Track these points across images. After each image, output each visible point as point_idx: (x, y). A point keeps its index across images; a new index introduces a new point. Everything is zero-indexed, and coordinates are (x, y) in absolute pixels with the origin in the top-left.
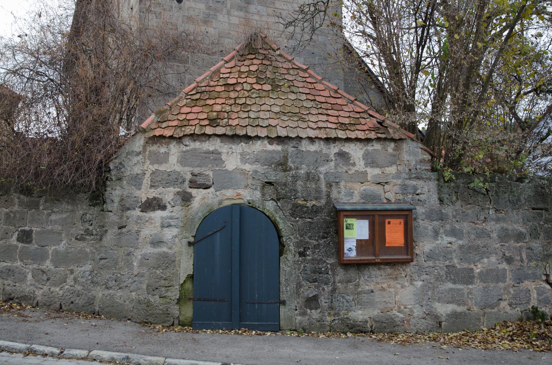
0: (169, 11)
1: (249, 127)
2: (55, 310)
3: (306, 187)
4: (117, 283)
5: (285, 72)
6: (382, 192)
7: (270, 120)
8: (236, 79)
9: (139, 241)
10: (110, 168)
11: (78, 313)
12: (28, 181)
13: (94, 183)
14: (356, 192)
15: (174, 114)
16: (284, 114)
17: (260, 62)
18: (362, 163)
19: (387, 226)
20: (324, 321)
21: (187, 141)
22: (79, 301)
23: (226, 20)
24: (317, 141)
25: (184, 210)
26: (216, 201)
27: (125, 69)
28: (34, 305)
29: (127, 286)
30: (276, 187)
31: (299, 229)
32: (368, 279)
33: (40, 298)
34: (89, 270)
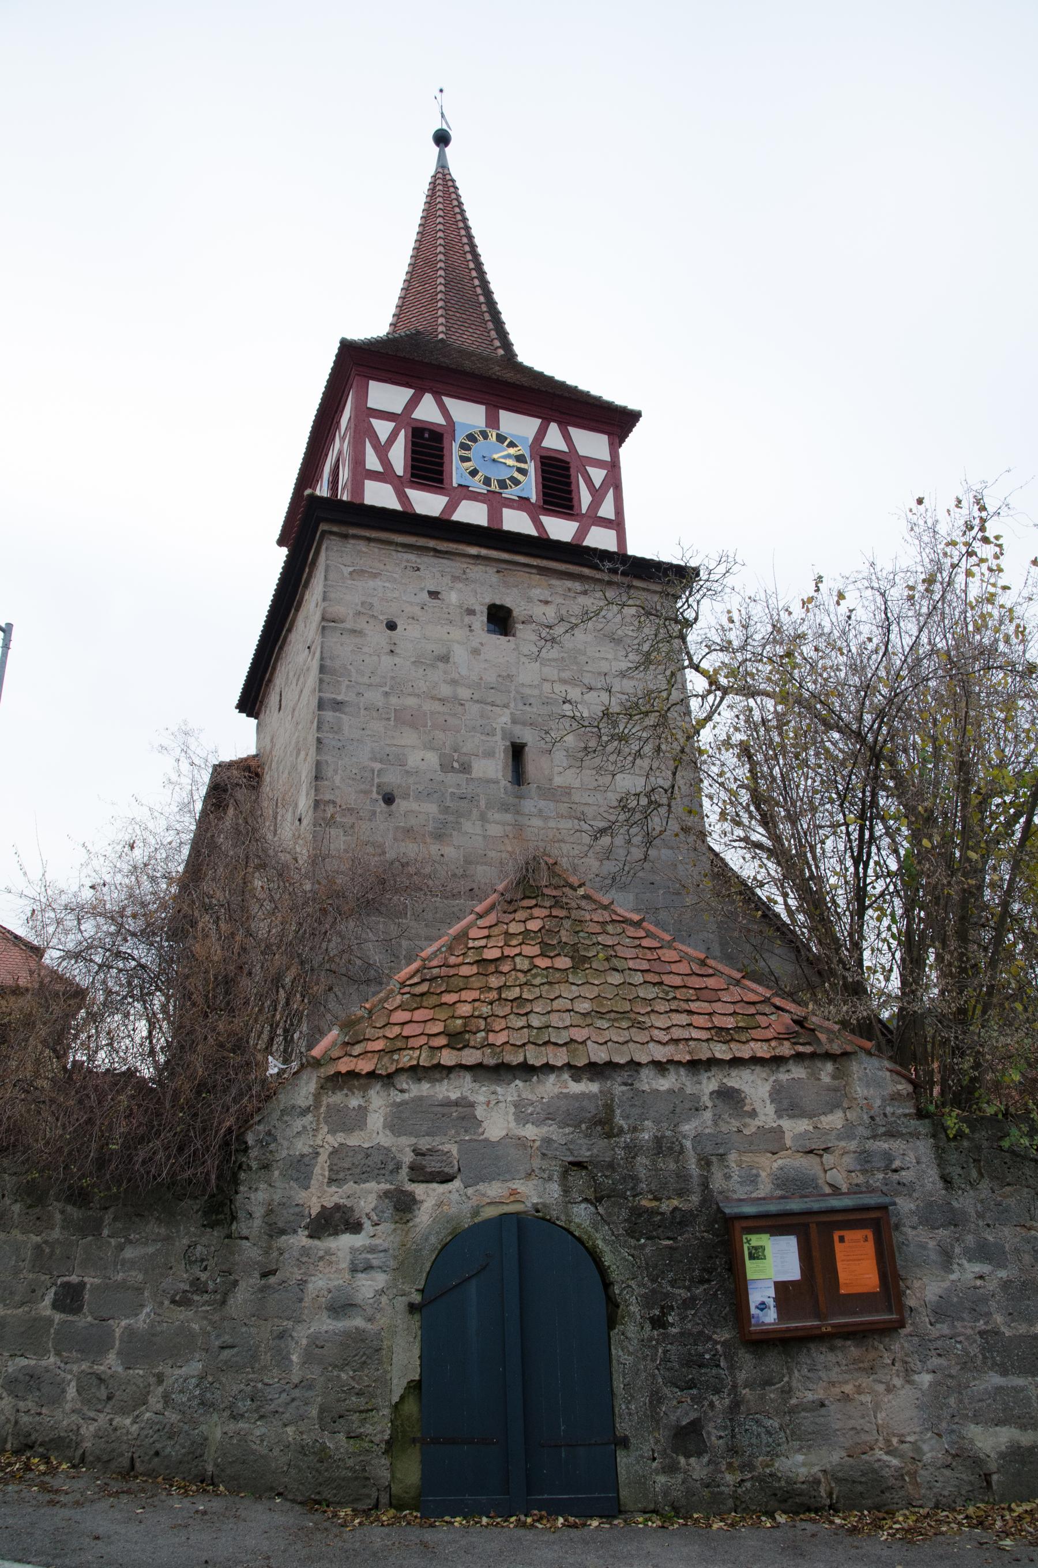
0: (370, 820)
1: (529, 1047)
2: (120, 1473)
3: (656, 1170)
4: (254, 1405)
5: (598, 929)
6: (817, 1170)
7: (571, 1029)
8: (500, 950)
9: (303, 1304)
10: (246, 1143)
11: (169, 1480)
12: (84, 1176)
13: (213, 1177)
14: (763, 1174)
15: (378, 1025)
16: (601, 1015)
17: (546, 912)
18: (770, 1109)
19: (838, 1247)
20: (719, 1486)
21: (403, 1081)
22: (172, 1450)
23: (479, 830)
24: (672, 1068)
25: (399, 1232)
26: (467, 1207)
27: (283, 936)
28: (76, 1461)
29: (277, 1412)
30: (591, 1172)
31: (647, 1264)
32: (809, 1375)
33: (89, 1444)
34: (196, 1373)
